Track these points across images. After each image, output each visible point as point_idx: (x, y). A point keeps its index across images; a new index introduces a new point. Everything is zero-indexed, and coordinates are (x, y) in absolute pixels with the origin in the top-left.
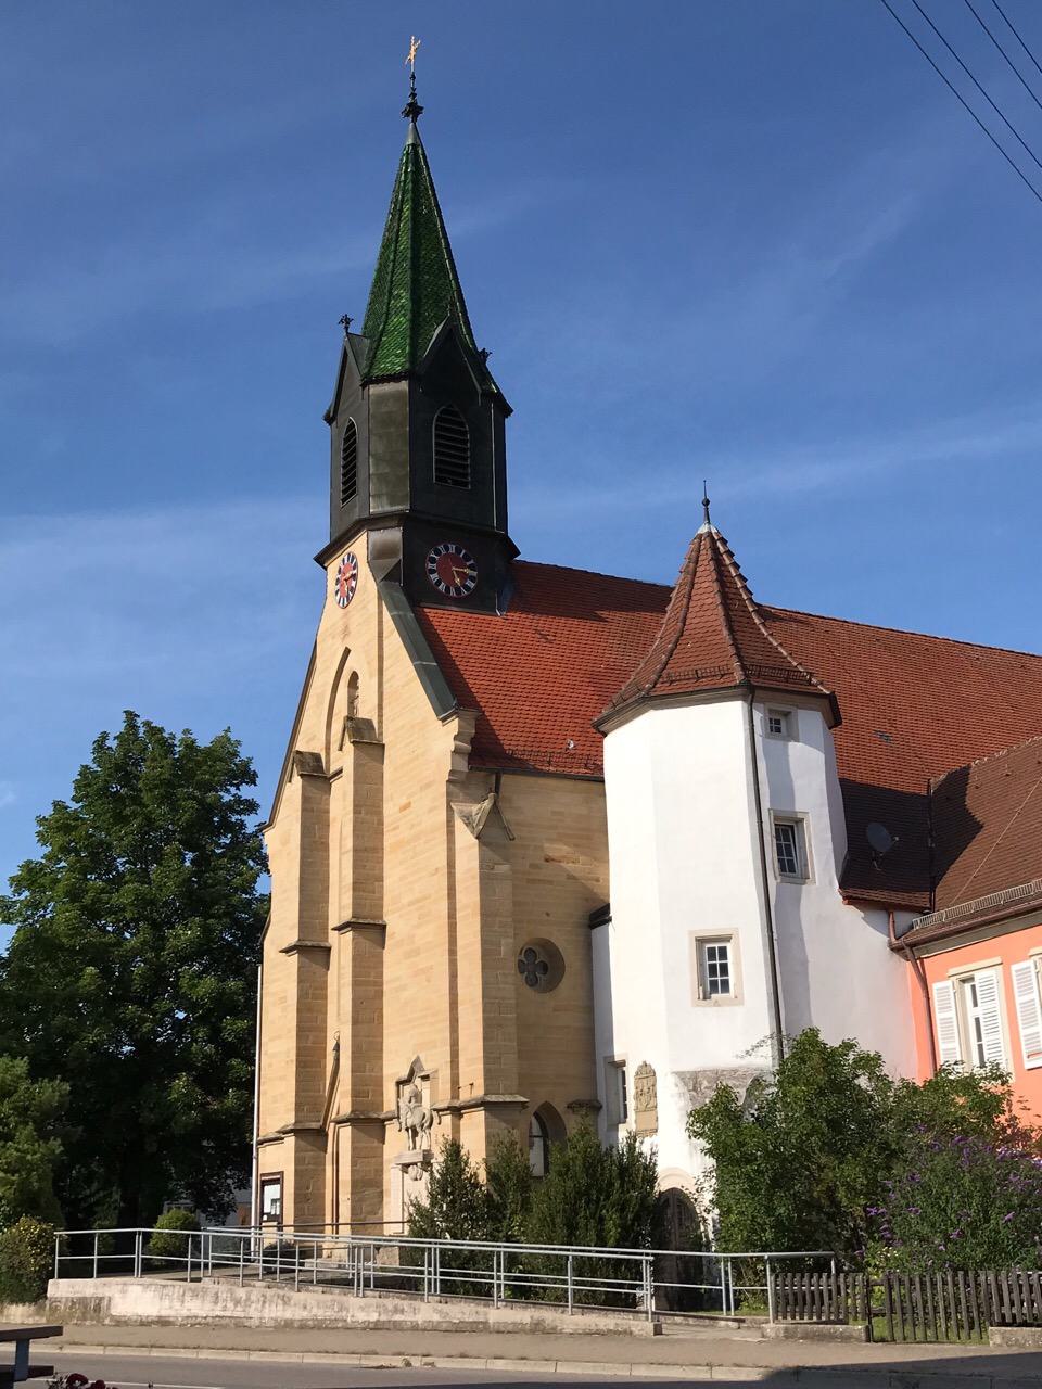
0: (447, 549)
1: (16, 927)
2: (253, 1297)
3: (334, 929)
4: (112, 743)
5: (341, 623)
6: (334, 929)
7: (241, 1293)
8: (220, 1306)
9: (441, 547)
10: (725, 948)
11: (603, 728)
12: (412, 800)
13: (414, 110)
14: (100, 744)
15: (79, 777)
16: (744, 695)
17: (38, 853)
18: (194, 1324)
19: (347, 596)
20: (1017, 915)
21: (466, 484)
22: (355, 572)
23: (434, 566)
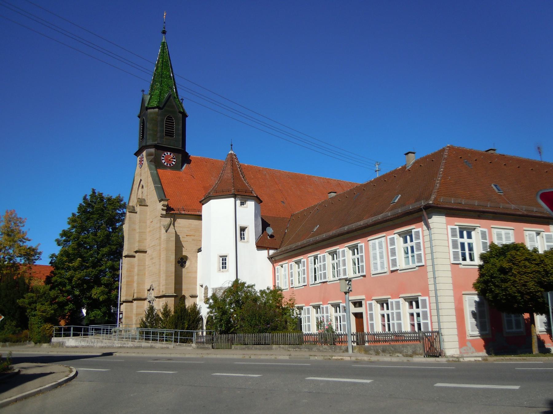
0: (167, 153)
1: (62, 247)
2: (95, 341)
3: (124, 256)
4: (88, 197)
5: (140, 172)
6: (124, 256)
7: (93, 340)
8: (88, 343)
9: (166, 153)
10: (226, 258)
11: (203, 202)
12: (153, 220)
14: (85, 198)
15: (79, 207)
16: (234, 196)
17: (67, 227)
18: (83, 347)
19: (141, 164)
20: (305, 247)
22: (143, 159)
23: (164, 158)
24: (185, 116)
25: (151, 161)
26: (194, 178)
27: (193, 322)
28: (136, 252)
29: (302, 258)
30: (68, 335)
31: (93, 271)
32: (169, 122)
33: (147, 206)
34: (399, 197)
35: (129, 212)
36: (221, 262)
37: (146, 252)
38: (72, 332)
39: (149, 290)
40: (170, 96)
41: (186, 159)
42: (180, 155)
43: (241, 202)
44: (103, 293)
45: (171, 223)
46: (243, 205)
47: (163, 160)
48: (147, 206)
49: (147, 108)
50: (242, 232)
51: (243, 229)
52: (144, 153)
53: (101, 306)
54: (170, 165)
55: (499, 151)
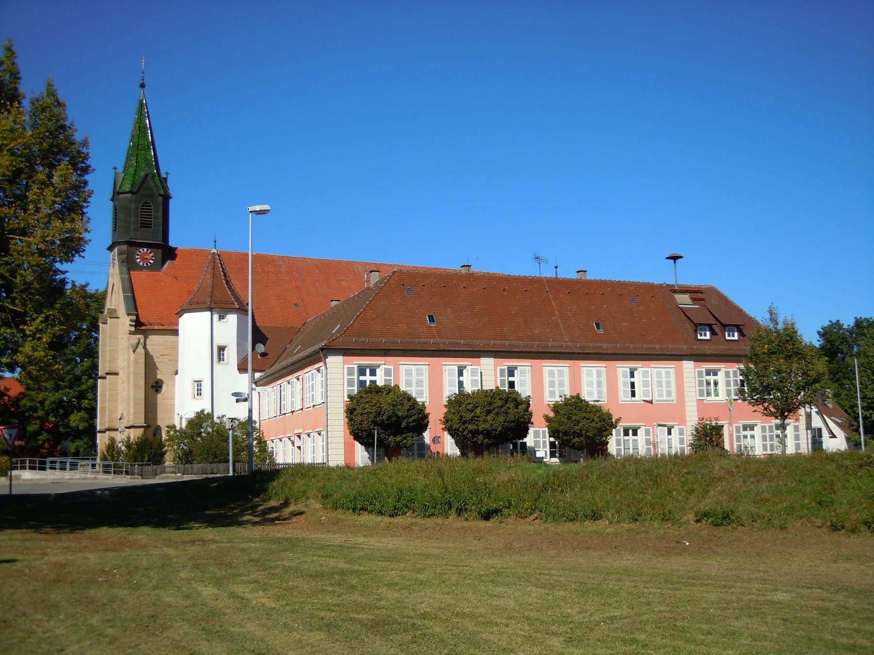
0: (143, 250)
13: (142, 86)
21: (151, 227)
23: (142, 252)
24: (167, 198)
25: (122, 262)
26: (178, 280)
27: (154, 456)
28: (107, 374)
29: (282, 381)
30: (23, 468)
31: (71, 393)
32: (146, 209)
33: (118, 318)
34: (338, 328)
35: (102, 323)
36: (196, 387)
37: (117, 374)
38: (27, 465)
39: (120, 419)
40: (146, 176)
41: (169, 253)
42: (160, 251)
43: (220, 316)
44: (82, 420)
45: (138, 344)
46: (223, 319)
47: (138, 258)
48: (118, 318)
49: (119, 193)
50: (222, 352)
51: (221, 349)
52: (116, 250)
53: (84, 436)
54: (147, 264)
55: (478, 268)
